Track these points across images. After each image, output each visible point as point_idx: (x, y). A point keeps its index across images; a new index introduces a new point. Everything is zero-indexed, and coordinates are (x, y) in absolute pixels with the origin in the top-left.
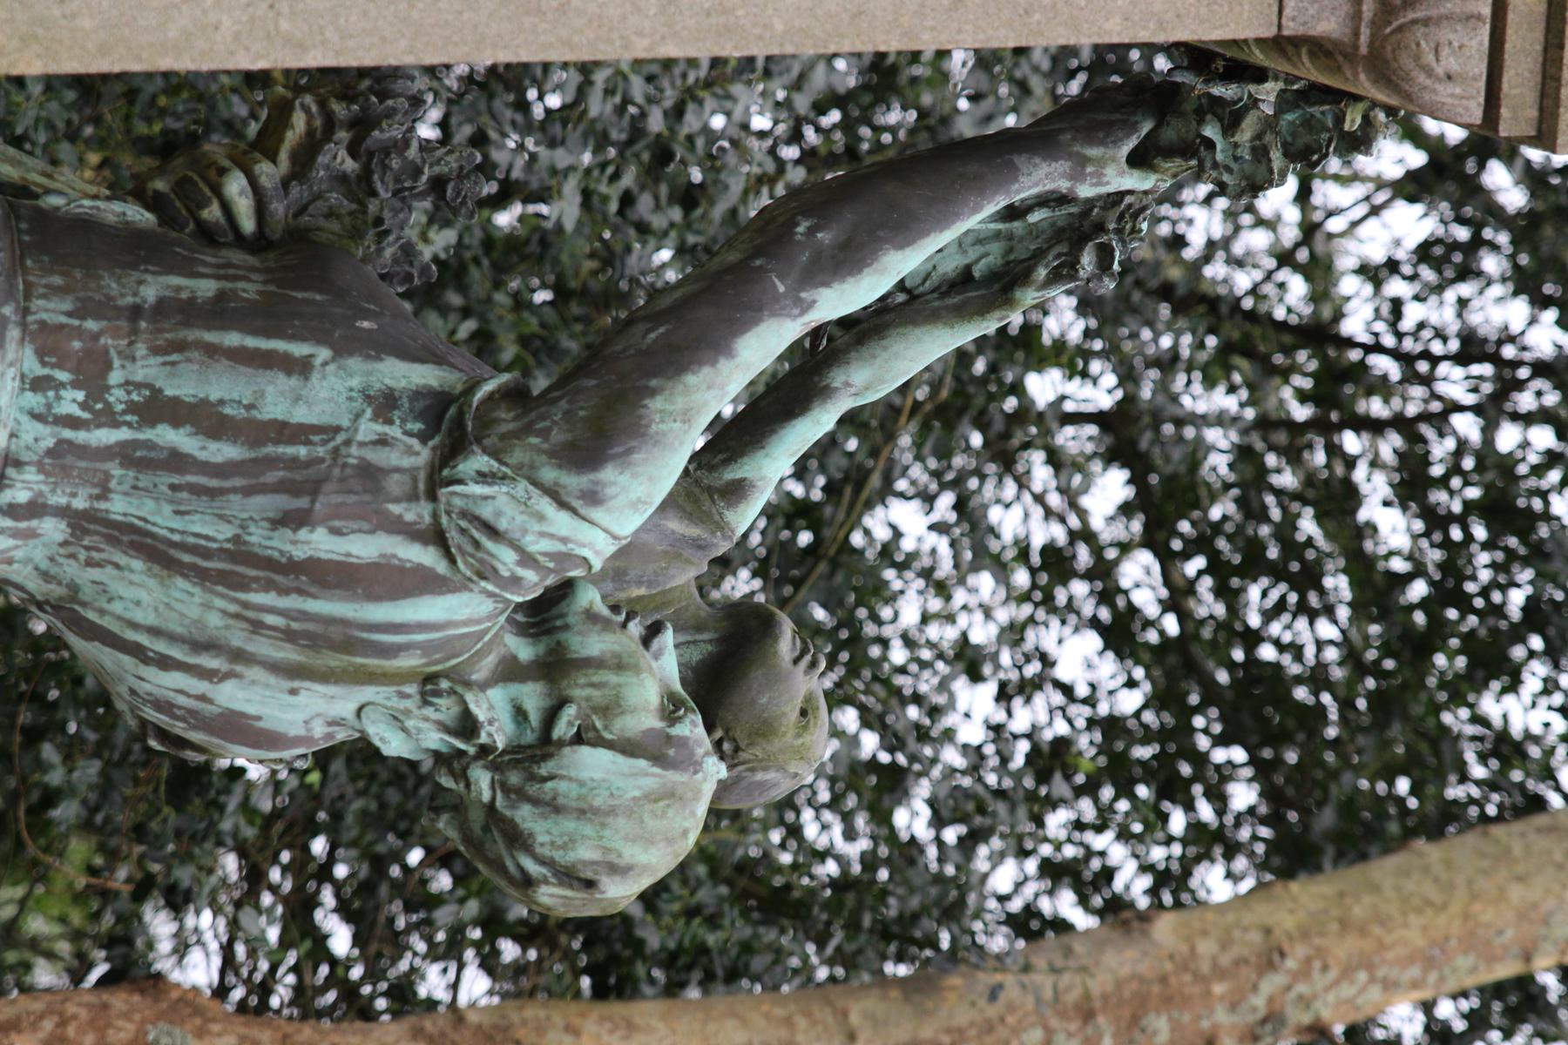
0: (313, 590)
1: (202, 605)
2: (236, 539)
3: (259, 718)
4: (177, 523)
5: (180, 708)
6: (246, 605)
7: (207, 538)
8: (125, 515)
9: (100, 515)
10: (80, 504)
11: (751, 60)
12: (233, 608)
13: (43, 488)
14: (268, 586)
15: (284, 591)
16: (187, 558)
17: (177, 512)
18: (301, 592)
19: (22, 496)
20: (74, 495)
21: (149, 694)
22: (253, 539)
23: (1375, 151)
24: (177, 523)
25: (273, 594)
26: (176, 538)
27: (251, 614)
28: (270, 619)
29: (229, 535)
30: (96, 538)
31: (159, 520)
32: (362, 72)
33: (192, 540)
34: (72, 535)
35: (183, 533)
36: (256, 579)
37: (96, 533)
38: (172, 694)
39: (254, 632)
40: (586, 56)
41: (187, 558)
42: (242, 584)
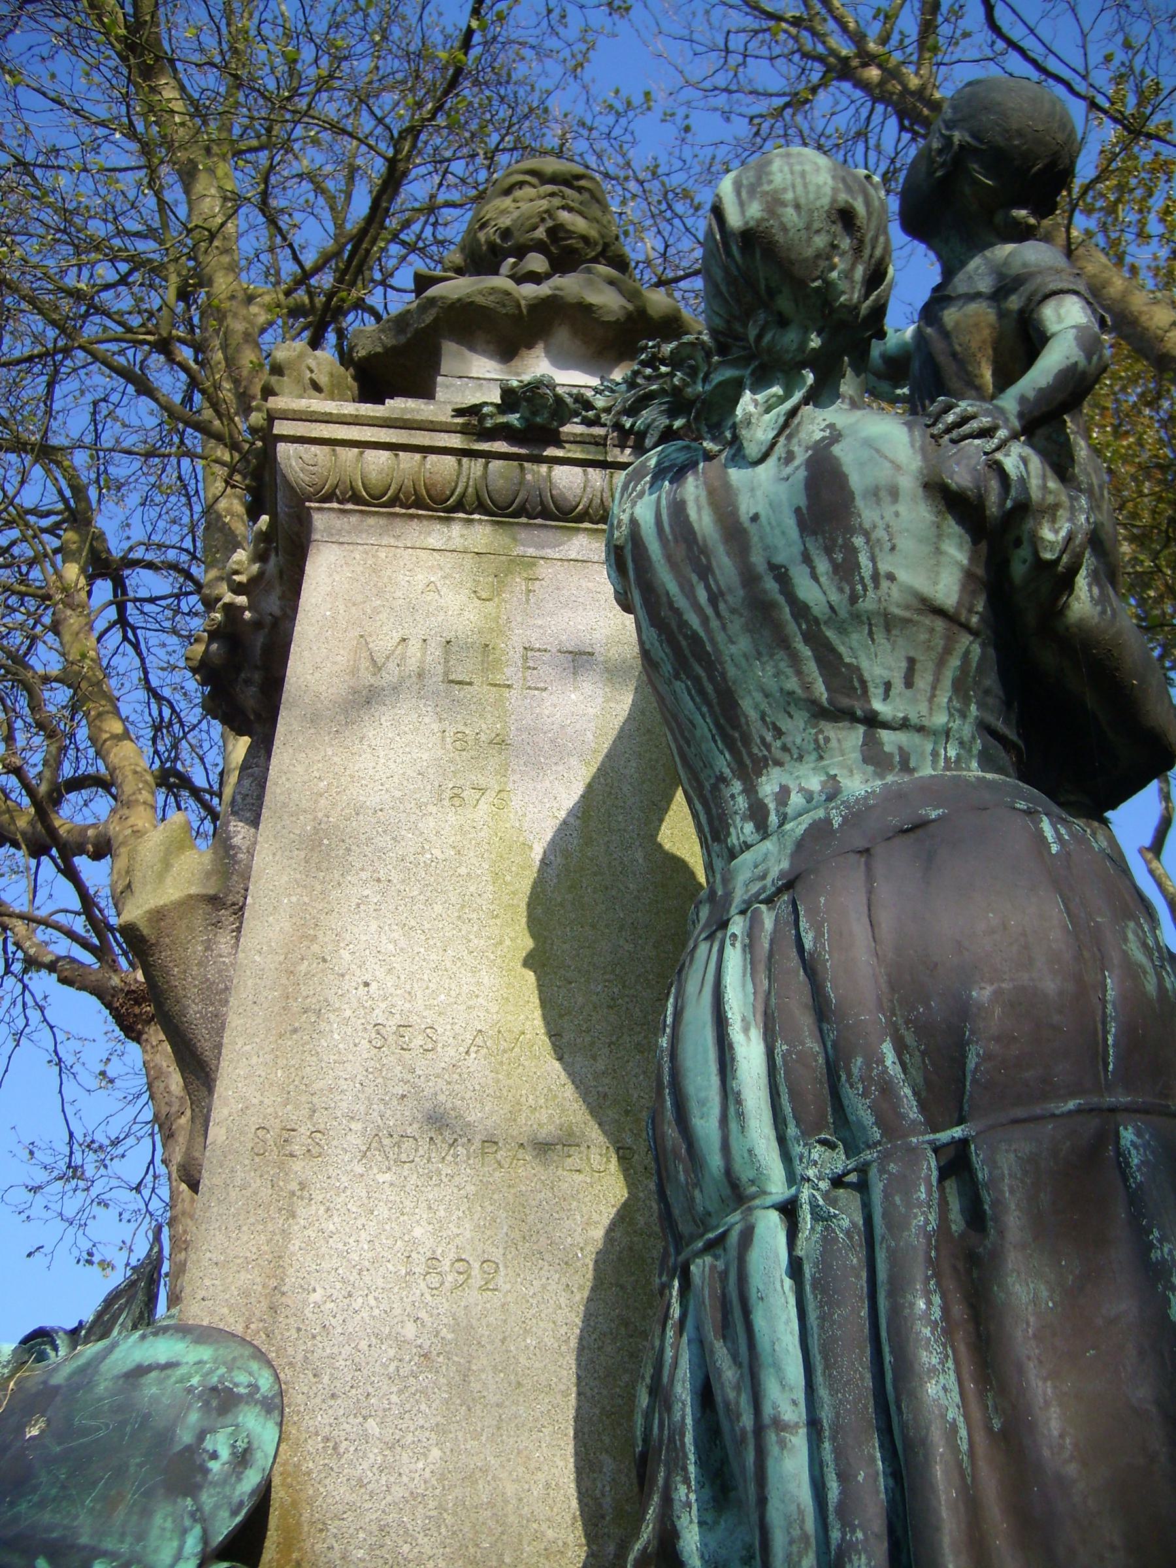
0: (664, 599)
1: (733, 643)
2: (677, 677)
3: (798, 510)
4: (698, 719)
5: (832, 561)
6: (705, 620)
7: (690, 694)
8: (722, 753)
9: (735, 767)
10: (737, 786)
11: (59, 980)
12: (715, 624)
13: (738, 818)
14: (683, 624)
15: (678, 612)
16: (709, 688)
17: (694, 726)
18: (671, 604)
19: (749, 827)
20: (733, 796)
21: (841, 590)
22: (669, 668)
23: (513, 363)
24: (698, 719)
25: (685, 617)
26: (705, 709)
27: (709, 611)
28: (702, 596)
29: (678, 683)
30: (755, 750)
31: (706, 730)
32: (220, 1053)
33: (698, 699)
34: (766, 766)
35: (699, 709)
36: (686, 636)
37: (751, 754)
38: (823, 579)
39: (722, 594)
40: (296, 1398)
41: (709, 688)
42: (695, 639)
